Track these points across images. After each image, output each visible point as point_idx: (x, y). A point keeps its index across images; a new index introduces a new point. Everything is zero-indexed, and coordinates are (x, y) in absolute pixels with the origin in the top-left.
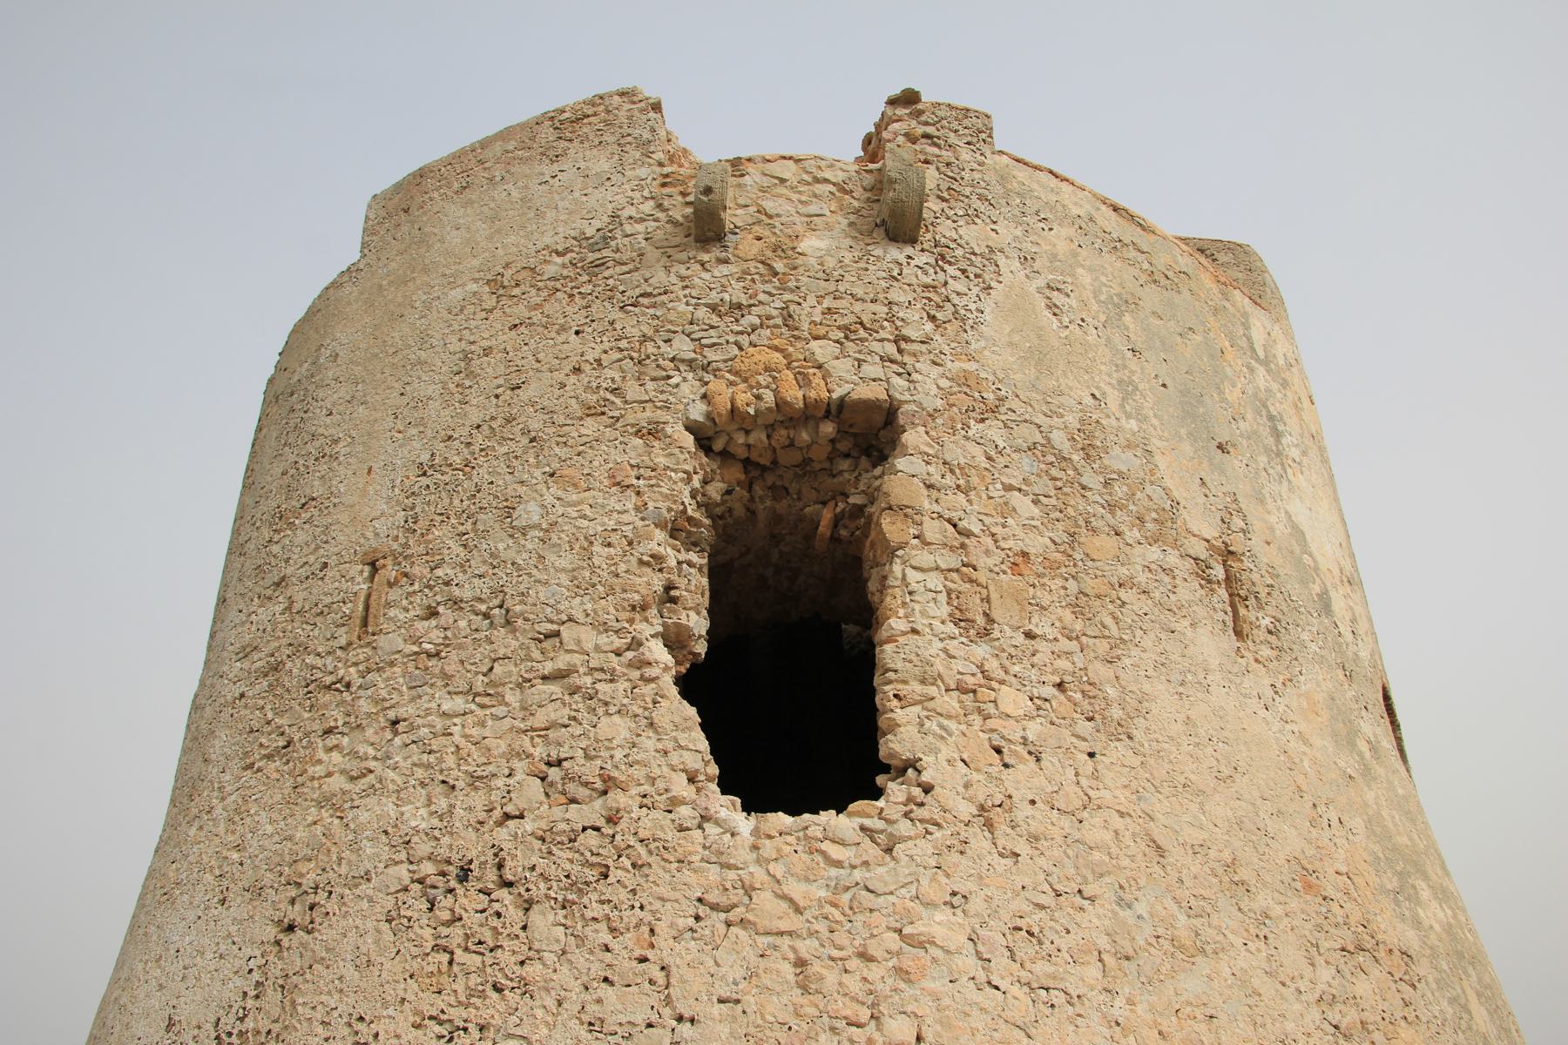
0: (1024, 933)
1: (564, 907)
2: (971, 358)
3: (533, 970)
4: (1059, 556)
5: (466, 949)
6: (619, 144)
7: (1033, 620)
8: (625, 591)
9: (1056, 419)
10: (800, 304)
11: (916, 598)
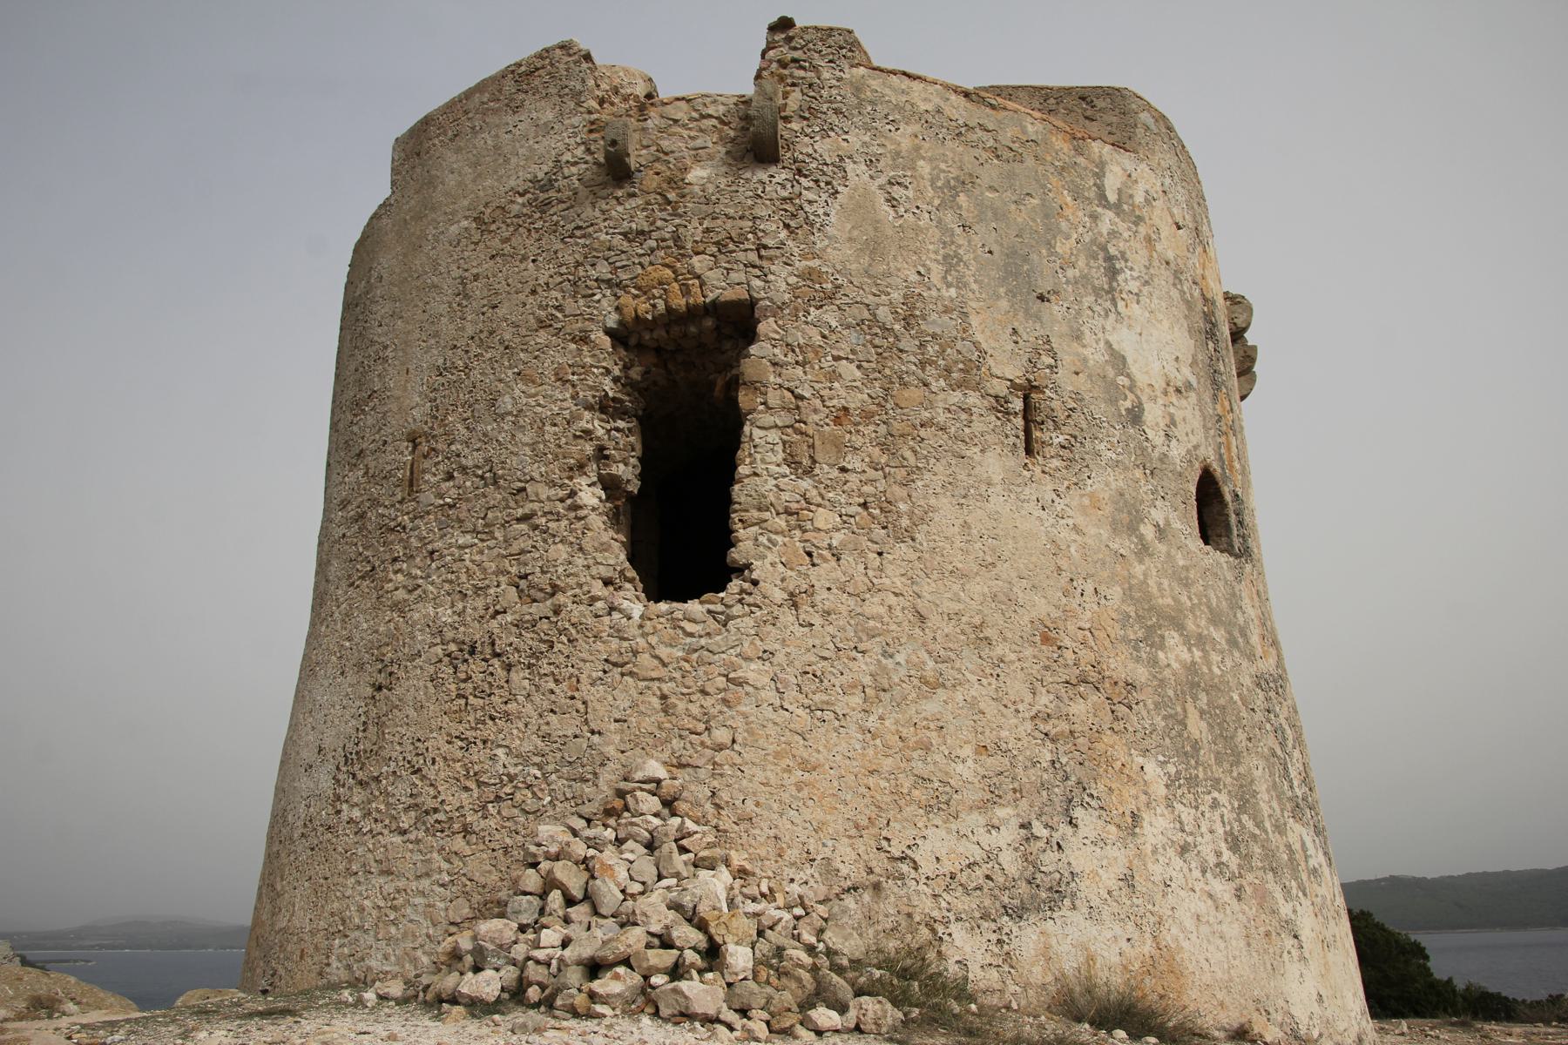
0: (810, 676)
1: (529, 668)
2: (815, 256)
3: (512, 707)
4: (874, 408)
5: (475, 696)
6: (560, 96)
7: (847, 459)
8: (565, 458)
9: (883, 297)
10: (686, 227)
11: (758, 450)
